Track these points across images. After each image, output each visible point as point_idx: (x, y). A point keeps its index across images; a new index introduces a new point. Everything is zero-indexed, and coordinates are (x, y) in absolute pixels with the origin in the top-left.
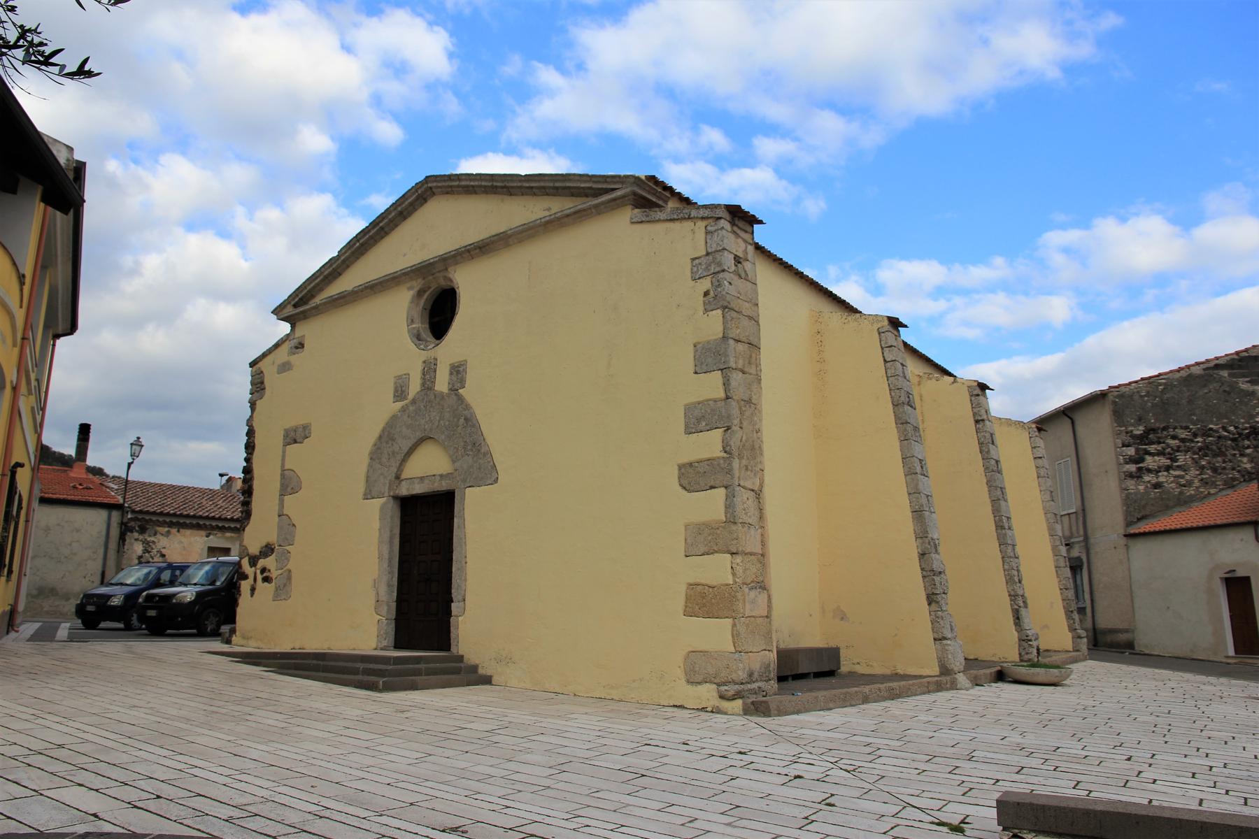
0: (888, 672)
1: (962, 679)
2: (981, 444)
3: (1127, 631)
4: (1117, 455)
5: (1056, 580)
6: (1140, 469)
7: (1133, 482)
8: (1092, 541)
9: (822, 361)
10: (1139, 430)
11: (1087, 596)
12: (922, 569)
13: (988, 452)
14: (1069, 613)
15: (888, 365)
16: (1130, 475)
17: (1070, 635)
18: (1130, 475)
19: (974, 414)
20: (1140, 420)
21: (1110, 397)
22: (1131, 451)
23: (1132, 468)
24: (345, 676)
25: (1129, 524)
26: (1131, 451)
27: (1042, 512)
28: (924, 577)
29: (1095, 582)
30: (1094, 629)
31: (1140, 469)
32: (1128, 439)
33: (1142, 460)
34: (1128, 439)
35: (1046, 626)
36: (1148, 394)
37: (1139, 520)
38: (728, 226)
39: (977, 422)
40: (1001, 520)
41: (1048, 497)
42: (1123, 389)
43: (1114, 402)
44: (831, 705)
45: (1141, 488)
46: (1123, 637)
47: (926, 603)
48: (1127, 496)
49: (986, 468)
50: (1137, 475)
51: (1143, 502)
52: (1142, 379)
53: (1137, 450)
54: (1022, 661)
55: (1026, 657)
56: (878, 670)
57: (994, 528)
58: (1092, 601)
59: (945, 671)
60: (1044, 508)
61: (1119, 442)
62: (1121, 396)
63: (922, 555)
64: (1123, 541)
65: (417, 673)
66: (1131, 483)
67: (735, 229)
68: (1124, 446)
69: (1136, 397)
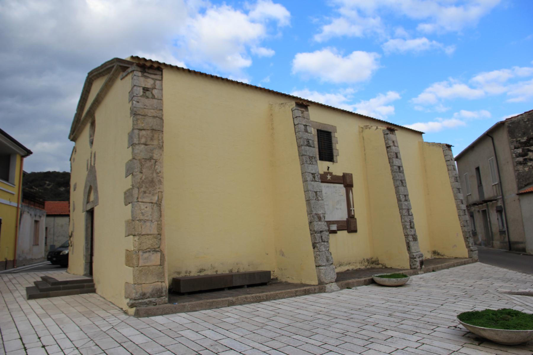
0: (299, 282)
1: (334, 286)
2: (389, 159)
3: (522, 243)
4: (512, 153)
5: (459, 222)
6: (525, 160)
7: (522, 166)
8: (505, 198)
9: (273, 129)
10: (524, 139)
11: (505, 225)
12: (311, 230)
13: (393, 162)
14: (466, 239)
15: (296, 126)
16: (520, 163)
17: (467, 250)
18: (520, 163)
19: (386, 144)
20: (524, 134)
21: (506, 124)
22: (520, 151)
23: (521, 159)
24: (78, 284)
25: (520, 188)
26: (520, 151)
27: (451, 188)
28: (311, 234)
29: (508, 218)
30: (509, 242)
31: (525, 160)
32: (517, 145)
33: (527, 155)
34: (517, 145)
35: (455, 246)
36: (528, 120)
37: (526, 186)
38: (140, 74)
39: (387, 147)
40: (400, 197)
41: (453, 180)
42: (513, 119)
43: (509, 127)
44: (197, 309)
45: (526, 169)
46: (521, 246)
47: (312, 248)
48: (518, 174)
49: (392, 171)
50: (524, 163)
51: (528, 177)
52: (525, 113)
53: (523, 150)
54: (411, 268)
55: (413, 267)
56: (296, 281)
57: (396, 201)
58: (507, 227)
59: (321, 283)
60: (452, 186)
61: (513, 147)
62: (513, 123)
63: (310, 223)
64: (517, 197)
65: (59, 289)
66: (520, 168)
67: (145, 74)
68: (515, 148)
69: (522, 122)
